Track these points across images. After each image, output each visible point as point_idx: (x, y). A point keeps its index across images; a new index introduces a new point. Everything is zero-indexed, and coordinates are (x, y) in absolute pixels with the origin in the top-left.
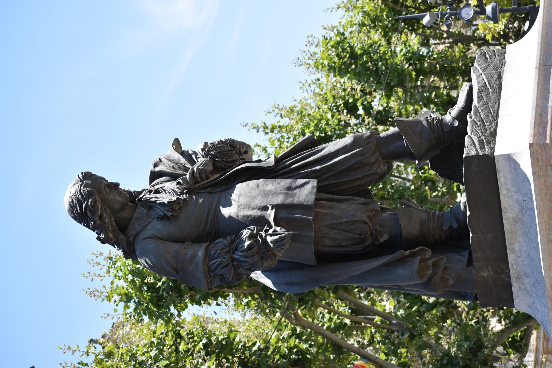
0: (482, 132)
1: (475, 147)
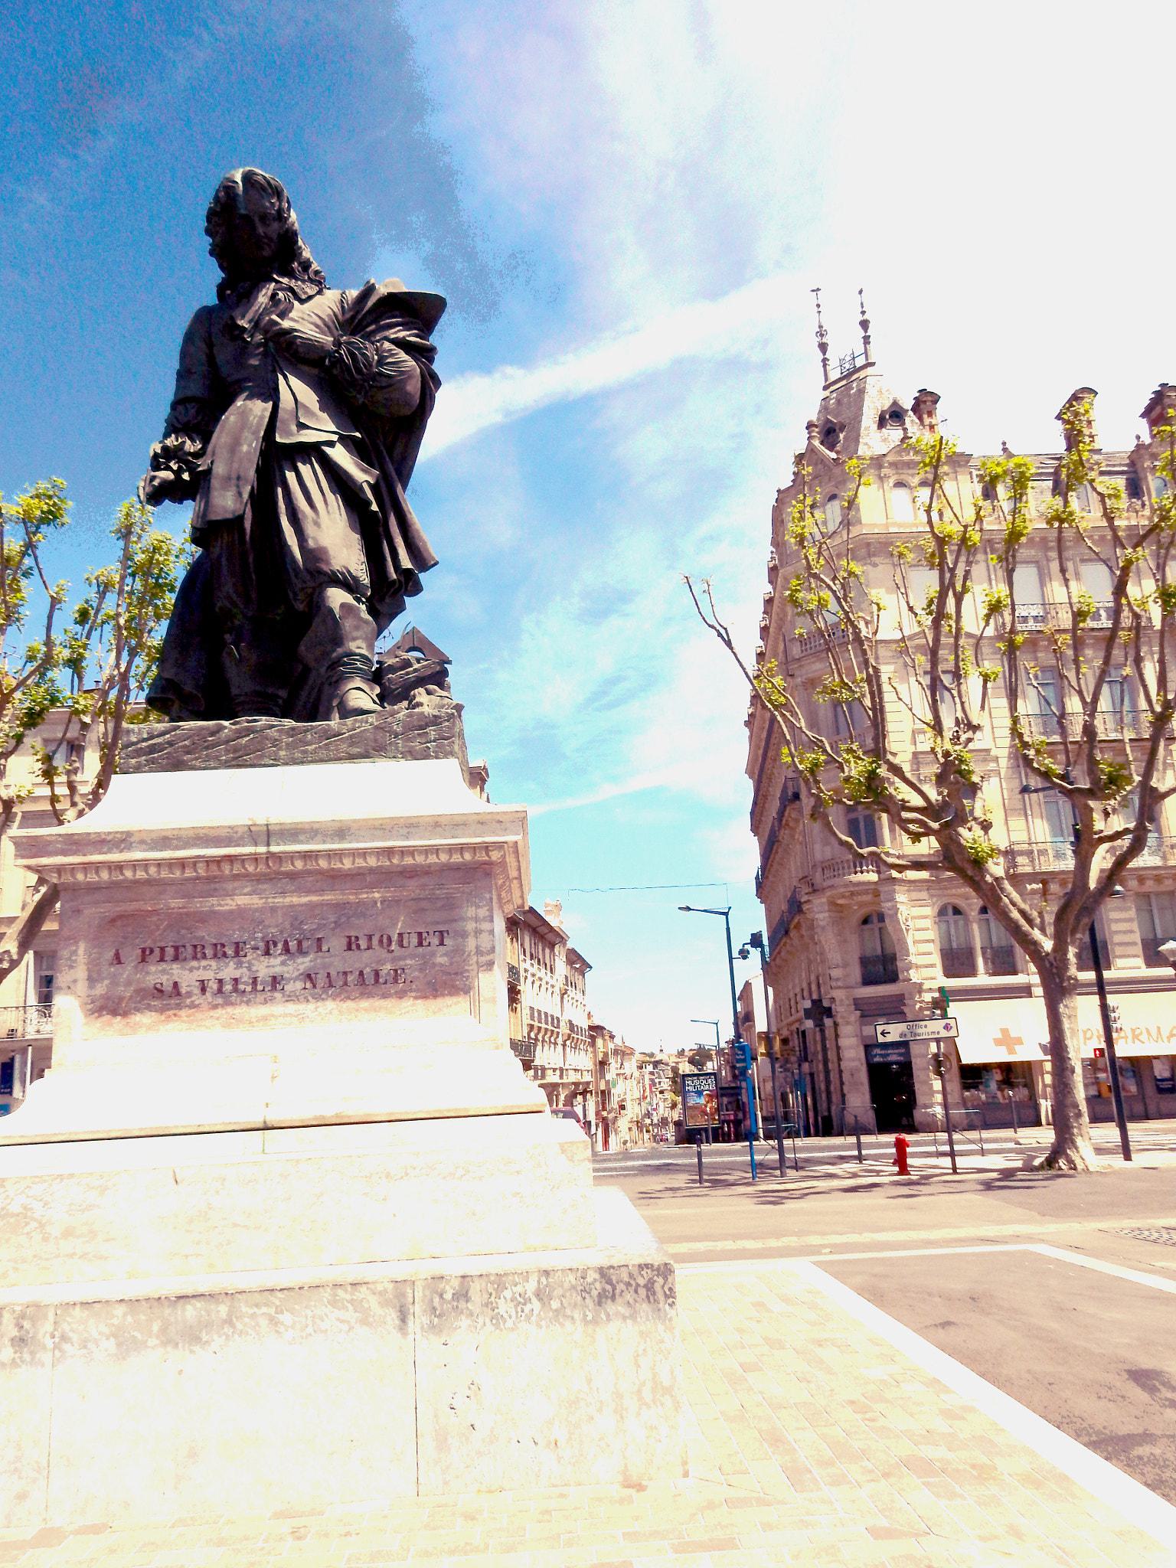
0: (185, 746)
1: (145, 740)
